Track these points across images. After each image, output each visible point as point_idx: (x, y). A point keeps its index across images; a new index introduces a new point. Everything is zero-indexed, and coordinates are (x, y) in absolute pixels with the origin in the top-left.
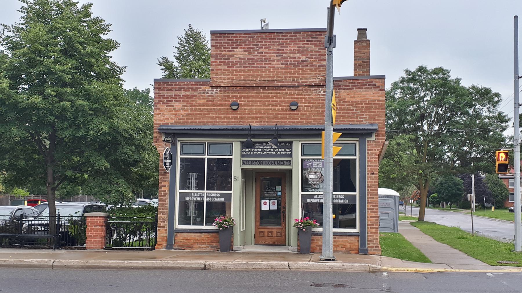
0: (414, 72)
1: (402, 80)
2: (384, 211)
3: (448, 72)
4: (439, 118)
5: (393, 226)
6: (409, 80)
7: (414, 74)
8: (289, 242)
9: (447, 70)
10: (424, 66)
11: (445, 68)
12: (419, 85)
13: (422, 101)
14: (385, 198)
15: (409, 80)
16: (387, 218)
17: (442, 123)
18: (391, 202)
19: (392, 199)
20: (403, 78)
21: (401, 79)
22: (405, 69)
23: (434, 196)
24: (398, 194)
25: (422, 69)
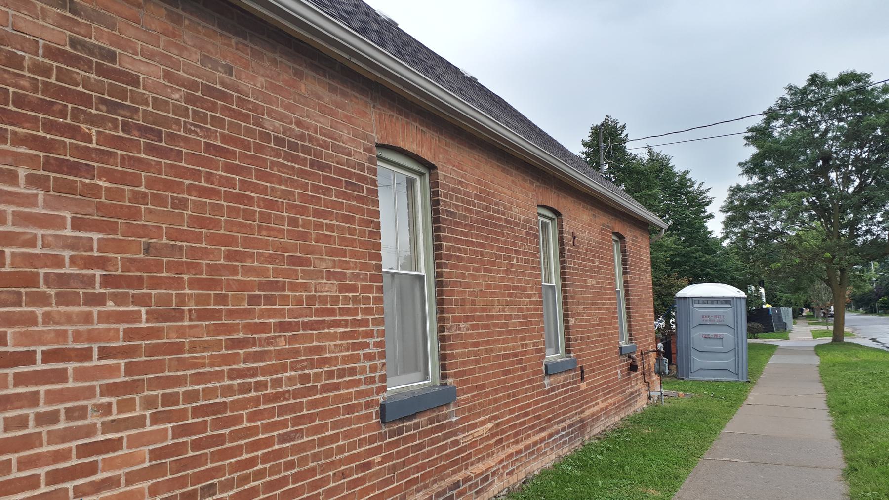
0: (805, 88)
1: (782, 103)
2: (711, 333)
3: (868, 76)
4: (861, 166)
5: (734, 367)
6: (797, 105)
7: (804, 92)
8: (707, 355)
9: (864, 74)
10: (820, 72)
11: (859, 72)
12: (816, 111)
13: (881, 206)
14: (722, 303)
15: (797, 105)
16: (719, 348)
17: (824, 124)
18: (727, 312)
19: (729, 306)
20: (782, 99)
21: (780, 102)
22: (786, 86)
23: (884, 300)
24: (743, 294)
25: (815, 79)
